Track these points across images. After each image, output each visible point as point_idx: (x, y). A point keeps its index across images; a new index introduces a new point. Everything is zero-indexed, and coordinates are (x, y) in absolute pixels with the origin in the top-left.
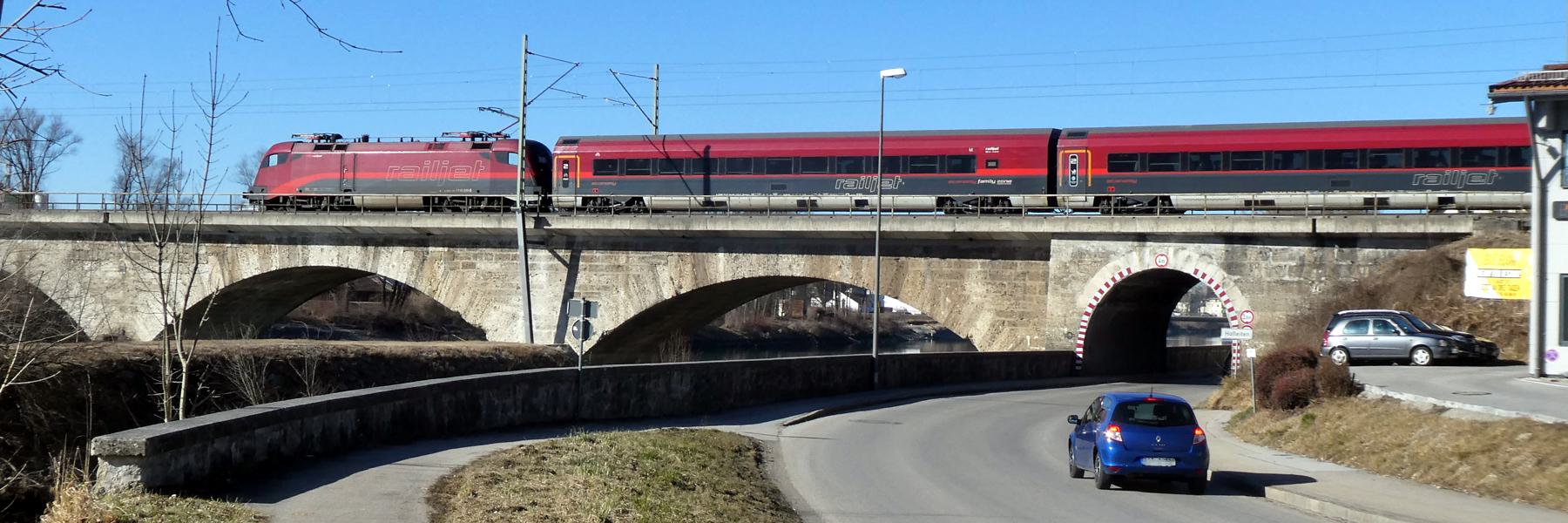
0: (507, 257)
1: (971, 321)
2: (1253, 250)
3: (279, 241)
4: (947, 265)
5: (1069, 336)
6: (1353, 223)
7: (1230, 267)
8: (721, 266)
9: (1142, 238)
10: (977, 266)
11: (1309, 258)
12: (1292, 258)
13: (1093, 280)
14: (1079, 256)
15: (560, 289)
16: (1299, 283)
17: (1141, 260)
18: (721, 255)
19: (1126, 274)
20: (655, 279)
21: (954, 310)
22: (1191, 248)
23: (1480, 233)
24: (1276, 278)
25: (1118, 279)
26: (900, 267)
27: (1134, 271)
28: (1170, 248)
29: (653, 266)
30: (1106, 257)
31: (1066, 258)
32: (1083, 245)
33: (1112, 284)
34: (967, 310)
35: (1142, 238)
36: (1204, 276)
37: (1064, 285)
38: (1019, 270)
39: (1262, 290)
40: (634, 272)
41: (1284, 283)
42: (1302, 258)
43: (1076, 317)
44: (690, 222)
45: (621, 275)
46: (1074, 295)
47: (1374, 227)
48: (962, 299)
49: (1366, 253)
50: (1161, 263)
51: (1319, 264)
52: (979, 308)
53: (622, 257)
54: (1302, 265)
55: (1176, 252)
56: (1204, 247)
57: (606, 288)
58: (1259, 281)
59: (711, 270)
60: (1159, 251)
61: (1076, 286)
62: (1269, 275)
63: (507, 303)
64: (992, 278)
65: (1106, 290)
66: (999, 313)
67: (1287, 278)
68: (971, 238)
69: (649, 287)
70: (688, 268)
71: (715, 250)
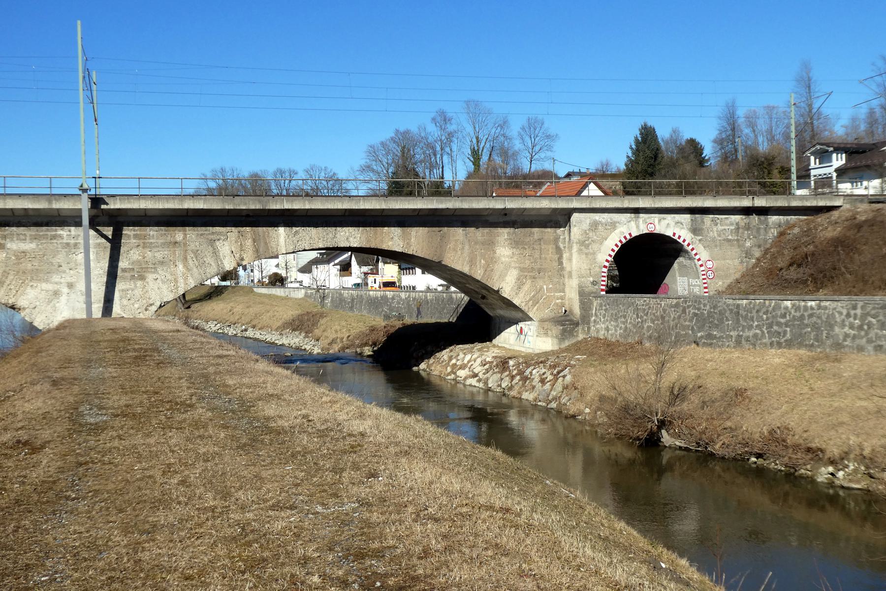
0: (45, 237)
1: (502, 277)
2: (708, 218)
3: (505, 225)
4: (479, 234)
5: (594, 283)
6: (776, 200)
7: (695, 231)
8: (282, 240)
9: (636, 211)
10: (504, 233)
11: (742, 224)
12: (732, 224)
13: (606, 243)
14: (595, 225)
15: (105, 264)
16: (738, 240)
17: (638, 227)
18: (281, 230)
19: (628, 237)
20: (215, 253)
21: (488, 269)
22: (670, 218)
23: (848, 206)
24: (723, 237)
25: (624, 241)
26: (443, 237)
27: (634, 235)
28: (655, 217)
29: (212, 242)
30: (613, 225)
31: (585, 226)
32: (597, 217)
33: (620, 245)
34: (498, 268)
35: (636, 211)
36: (679, 237)
37: (587, 246)
38: (536, 237)
39: (716, 246)
40: (192, 246)
41: (729, 241)
42: (737, 224)
43: (597, 269)
44: (590, 203)
45: (178, 252)
46: (594, 253)
47: (305, 205)
48: (492, 260)
49: (774, 219)
50: (651, 229)
51: (748, 227)
52: (508, 267)
53: (179, 234)
54: (738, 229)
55: (660, 221)
56: (678, 217)
57: (162, 263)
58: (714, 240)
59: (273, 244)
60: (649, 221)
61: (595, 246)
62: (719, 236)
63: (47, 281)
64: (515, 243)
65: (616, 249)
66: (522, 270)
67: (730, 237)
68: (505, 212)
69: (209, 260)
70: (249, 242)
71: (275, 225)
